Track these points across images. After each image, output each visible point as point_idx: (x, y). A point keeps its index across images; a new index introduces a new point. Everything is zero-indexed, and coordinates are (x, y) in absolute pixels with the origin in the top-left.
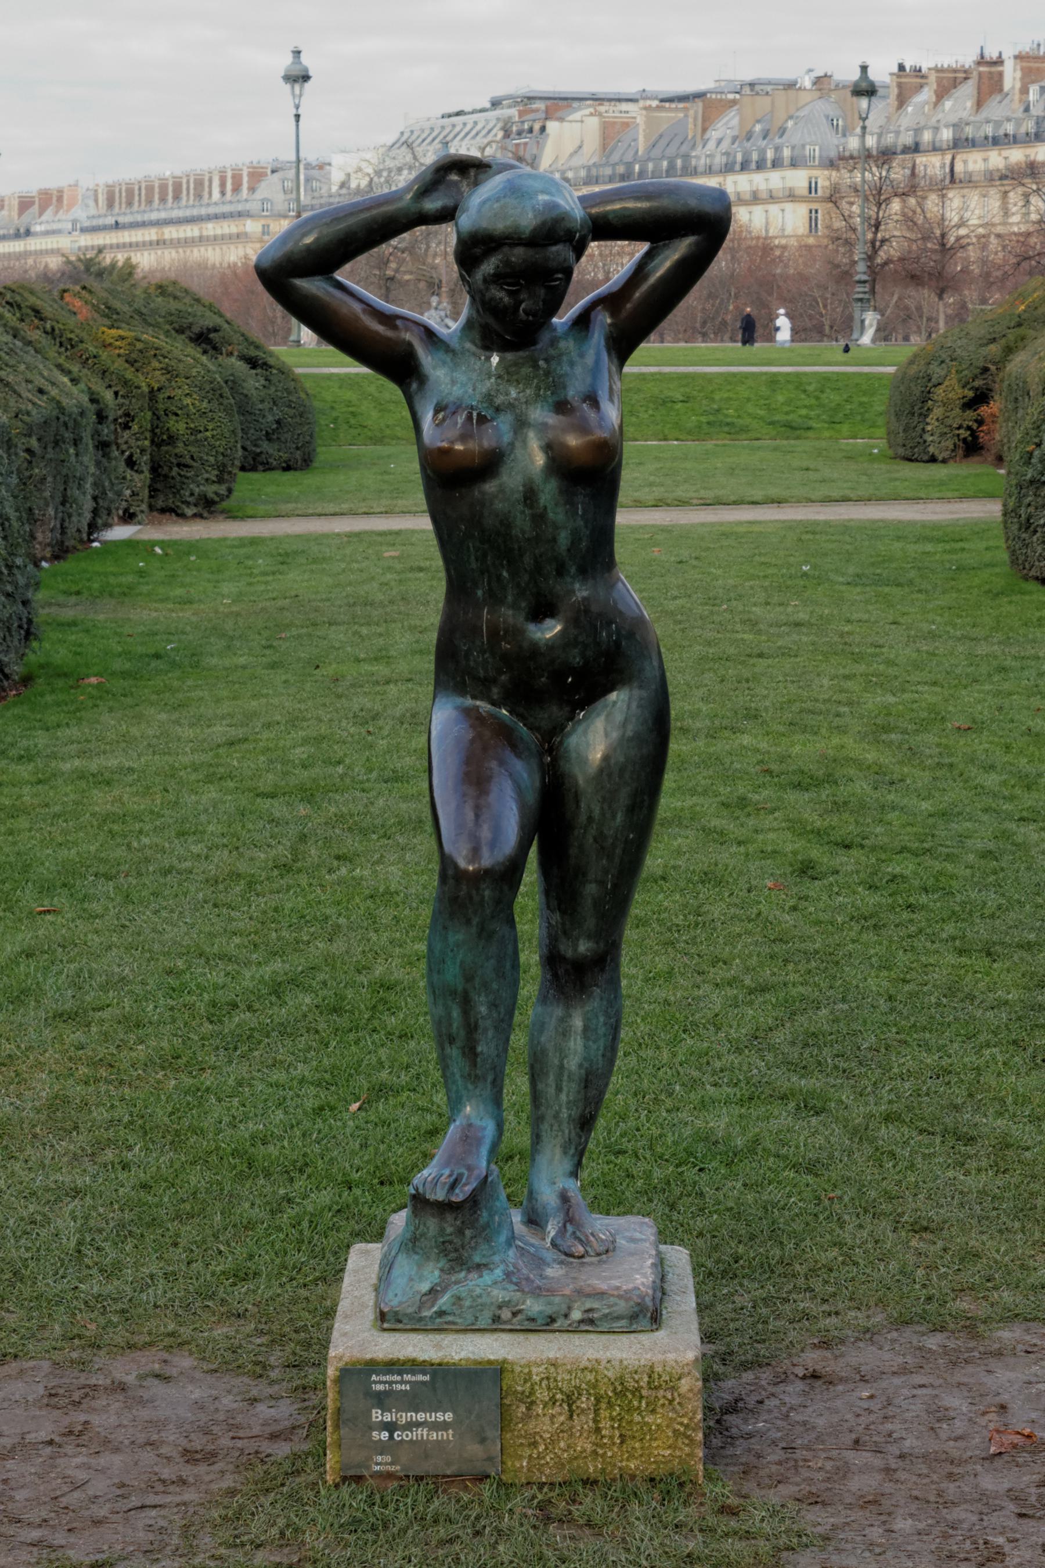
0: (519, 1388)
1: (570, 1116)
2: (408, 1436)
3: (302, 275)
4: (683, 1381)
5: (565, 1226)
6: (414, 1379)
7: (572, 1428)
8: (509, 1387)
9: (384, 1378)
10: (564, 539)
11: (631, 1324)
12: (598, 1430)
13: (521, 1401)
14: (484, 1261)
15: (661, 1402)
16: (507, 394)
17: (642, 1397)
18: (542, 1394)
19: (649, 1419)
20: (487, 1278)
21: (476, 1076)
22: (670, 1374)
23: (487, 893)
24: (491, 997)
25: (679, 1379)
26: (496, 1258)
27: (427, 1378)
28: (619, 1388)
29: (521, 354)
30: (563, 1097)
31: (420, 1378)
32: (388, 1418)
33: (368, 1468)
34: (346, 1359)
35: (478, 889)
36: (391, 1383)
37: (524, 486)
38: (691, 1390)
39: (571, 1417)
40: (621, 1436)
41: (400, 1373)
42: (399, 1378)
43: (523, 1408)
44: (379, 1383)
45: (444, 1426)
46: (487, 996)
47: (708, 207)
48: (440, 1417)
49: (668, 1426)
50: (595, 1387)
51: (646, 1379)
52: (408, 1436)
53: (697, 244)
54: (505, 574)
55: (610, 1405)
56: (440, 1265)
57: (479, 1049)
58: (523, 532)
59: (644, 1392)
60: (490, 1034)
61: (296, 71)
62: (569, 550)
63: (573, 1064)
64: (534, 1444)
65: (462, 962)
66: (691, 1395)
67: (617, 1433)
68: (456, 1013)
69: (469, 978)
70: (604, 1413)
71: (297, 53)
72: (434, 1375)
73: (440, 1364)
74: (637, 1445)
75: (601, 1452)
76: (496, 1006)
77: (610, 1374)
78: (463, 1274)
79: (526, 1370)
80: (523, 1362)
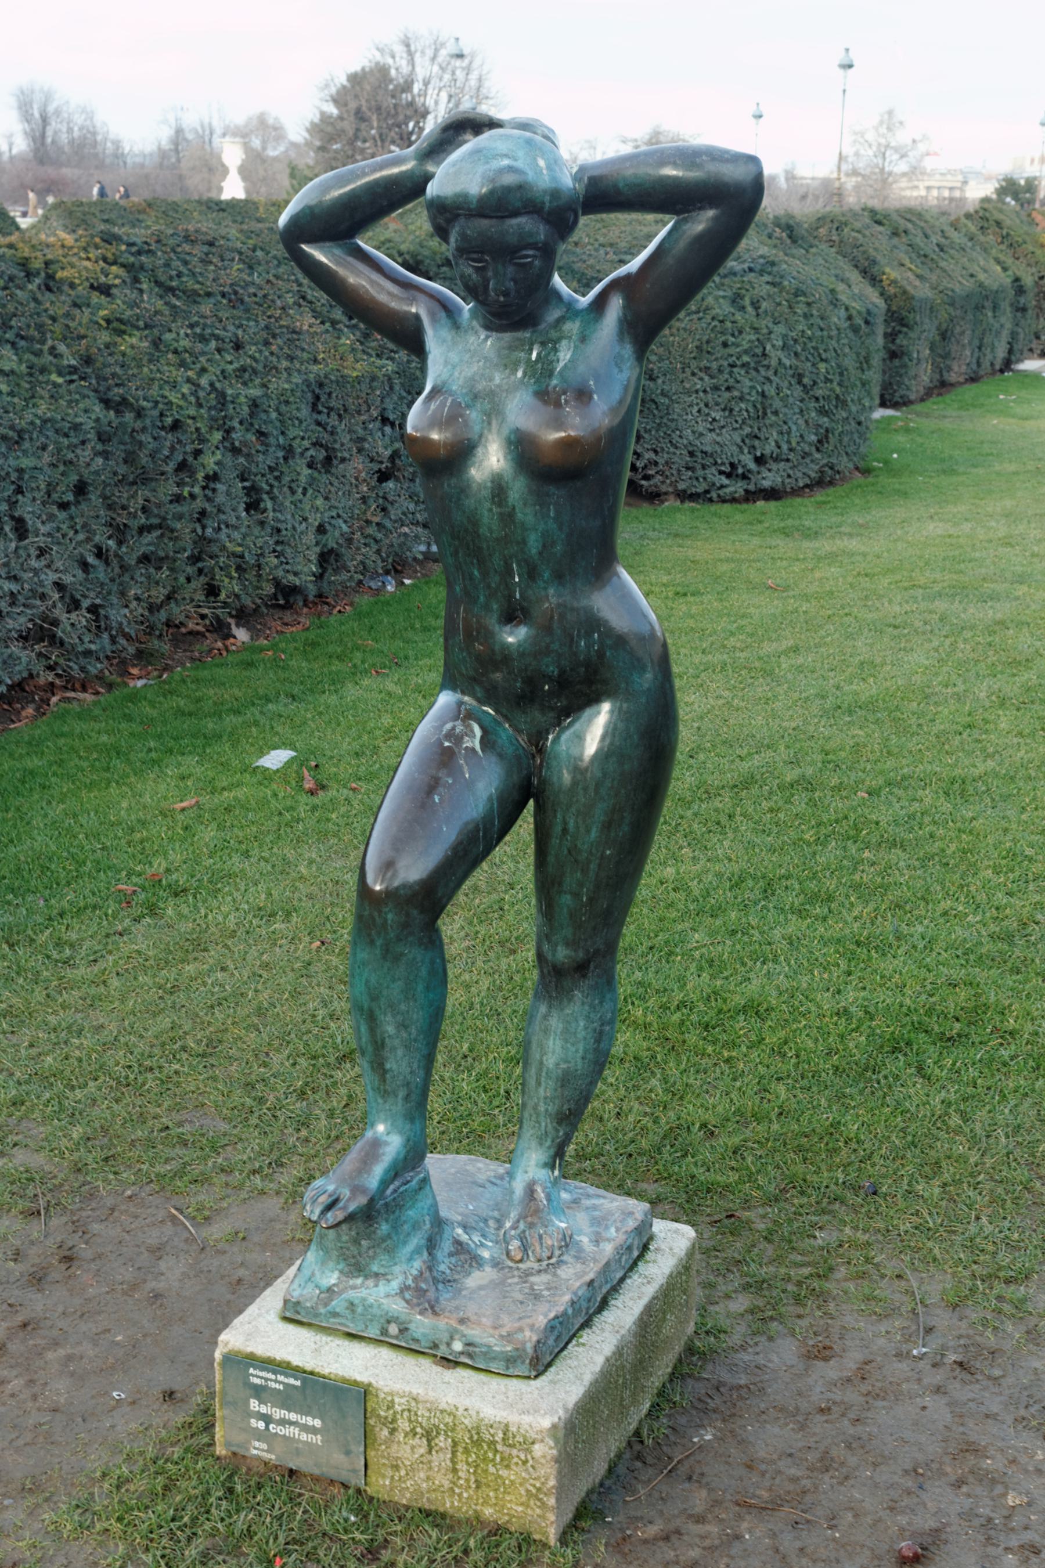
0: (382, 1413)
1: (547, 1110)
2: (281, 1430)
3: (308, 242)
4: (536, 1446)
5: (518, 1221)
6: (286, 1381)
7: (430, 1462)
8: (374, 1410)
9: (261, 1374)
10: (534, 543)
11: (508, 1368)
12: (455, 1470)
13: (384, 1424)
14: (382, 1271)
15: (515, 1460)
16: (491, 380)
17: (496, 1451)
18: (403, 1425)
19: (504, 1473)
20: (383, 1288)
21: (385, 1091)
22: (524, 1437)
23: (390, 916)
24: (400, 1018)
25: (533, 1443)
26: (397, 1269)
27: (298, 1383)
28: (475, 1437)
29: (519, 334)
30: (541, 1091)
31: (292, 1381)
32: (264, 1409)
33: (248, 1450)
34: (230, 1347)
35: (380, 912)
36: (266, 1380)
37: (492, 482)
38: (544, 1457)
39: (430, 1452)
40: (476, 1481)
41: (275, 1373)
42: (273, 1377)
43: (385, 1432)
44: (257, 1377)
45: (313, 1430)
46: (394, 1016)
47: (737, 173)
48: (309, 1421)
49: (521, 1484)
50: (453, 1430)
51: (501, 1435)
52: (281, 1430)
53: (715, 219)
54: (476, 573)
55: (466, 1451)
56: (340, 1267)
57: (388, 1066)
58: (491, 531)
59: (499, 1447)
60: (400, 1053)
61: (847, 62)
62: (540, 553)
63: (550, 1061)
64: (396, 1468)
65: (367, 982)
66: (543, 1461)
67: (473, 1479)
68: (364, 1029)
69: (374, 998)
70: (460, 1456)
71: (847, 50)
72: (304, 1381)
73: (312, 1373)
74: (491, 1494)
75: (457, 1490)
76: (406, 1027)
77: (466, 1422)
78: (359, 1281)
79: (389, 1398)
80: (386, 1390)
